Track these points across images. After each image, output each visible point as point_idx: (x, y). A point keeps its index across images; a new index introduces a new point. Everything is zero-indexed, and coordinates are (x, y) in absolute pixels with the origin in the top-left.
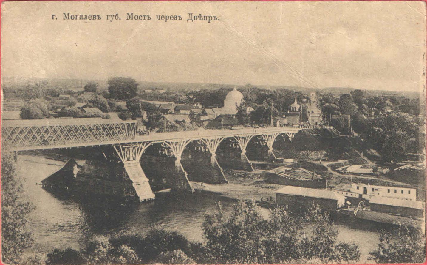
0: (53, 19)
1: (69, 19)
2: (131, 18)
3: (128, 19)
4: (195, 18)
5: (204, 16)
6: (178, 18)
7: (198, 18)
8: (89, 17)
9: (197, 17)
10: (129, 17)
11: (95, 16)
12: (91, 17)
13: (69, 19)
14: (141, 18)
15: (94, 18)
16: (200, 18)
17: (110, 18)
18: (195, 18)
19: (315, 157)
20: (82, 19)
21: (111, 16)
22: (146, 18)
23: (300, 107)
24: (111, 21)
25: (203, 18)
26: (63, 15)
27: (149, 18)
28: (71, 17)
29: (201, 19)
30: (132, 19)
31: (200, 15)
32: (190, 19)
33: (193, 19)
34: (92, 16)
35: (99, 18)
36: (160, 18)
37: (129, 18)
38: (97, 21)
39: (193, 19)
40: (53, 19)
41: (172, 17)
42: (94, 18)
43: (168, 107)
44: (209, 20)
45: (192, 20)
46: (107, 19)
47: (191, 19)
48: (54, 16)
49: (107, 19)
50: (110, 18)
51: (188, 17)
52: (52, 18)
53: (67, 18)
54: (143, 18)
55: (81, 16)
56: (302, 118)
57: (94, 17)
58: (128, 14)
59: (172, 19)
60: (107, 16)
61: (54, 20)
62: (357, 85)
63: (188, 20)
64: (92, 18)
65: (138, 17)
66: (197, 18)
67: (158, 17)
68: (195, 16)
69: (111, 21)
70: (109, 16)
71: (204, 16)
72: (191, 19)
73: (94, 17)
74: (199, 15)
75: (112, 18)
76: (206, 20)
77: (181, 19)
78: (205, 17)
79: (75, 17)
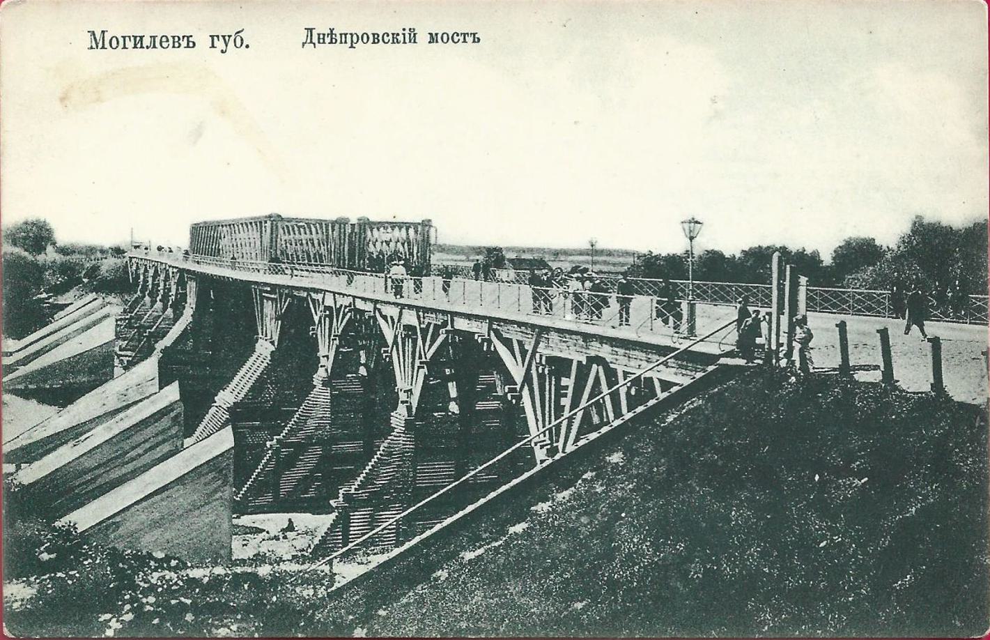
2: (100, 45)
3: (92, 48)
4: (322, 38)
5: (341, 34)
7: (328, 40)
8: (161, 42)
9: (324, 35)
10: (94, 42)
11: (176, 39)
12: (168, 41)
13: (103, 47)
14: (456, 39)
15: (177, 45)
16: (332, 39)
17: (220, 44)
18: (322, 38)
19: (249, 553)
20: (142, 47)
22: (469, 39)
23: (12, 474)
25: (338, 38)
26: (429, 36)
28: (368, 38)
29: (334, 41)
30: (437, 42)
31: (332, 30)
32: (309, 41)
33: (315, 39)
34: (171, 40)
35: (191, 45)
36: (380, 38)
37: (94, 46)
38: (183, 52)
39: (315, 39)
41: (164, 39)
42: (177, 45)
44: (352, 41)
45: (314, 44)
47: (311, 42)
48: (215, 38)
49: (213, 46)
50: (220, 44)
53: (100, 45)
54: (462, 38)
57: (176, 41)
58: (431, 34)
59: (165, 45)
60: (212, 37)
63: (304, 44)
65: (358, 36)
66: (324, 39)
67: (191, 44)
68: (319, 35)
69: (477, 40)
71: (341, 34)
72: (311, 42)
73: (176, 41)
74: (329, 32)
76: (346, 42)
78: (343, 36)
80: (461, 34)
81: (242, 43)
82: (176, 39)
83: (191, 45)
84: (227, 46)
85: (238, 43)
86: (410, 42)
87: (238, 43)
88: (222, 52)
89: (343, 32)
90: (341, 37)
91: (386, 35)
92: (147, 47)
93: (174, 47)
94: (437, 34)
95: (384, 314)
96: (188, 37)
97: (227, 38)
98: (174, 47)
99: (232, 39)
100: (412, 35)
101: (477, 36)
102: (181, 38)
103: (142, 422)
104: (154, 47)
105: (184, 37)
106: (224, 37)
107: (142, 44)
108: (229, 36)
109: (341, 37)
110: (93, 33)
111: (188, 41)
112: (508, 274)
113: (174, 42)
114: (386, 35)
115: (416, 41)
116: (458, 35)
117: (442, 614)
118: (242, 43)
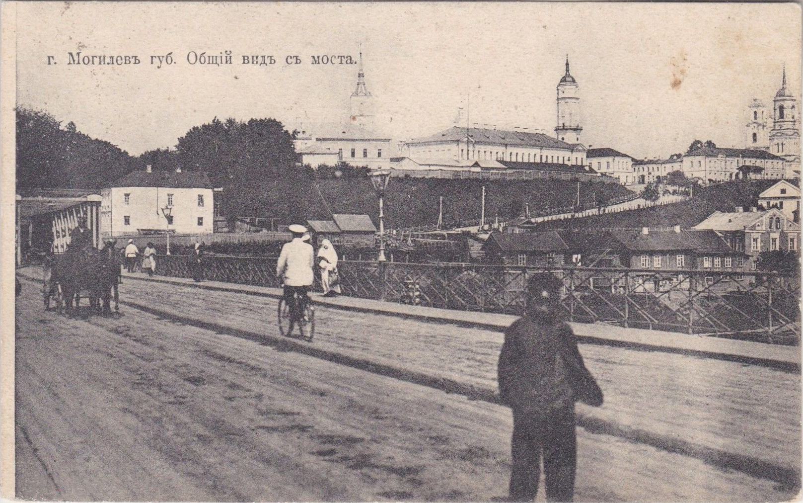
0: (49, 63)
1: (79, 63)
3: (70, 64)
6: (268, 61)
8: (117, 60)
10: (71, 59)
11: (127, 58)
12: (122, 59)
13: (79, 63)
15: (128, 62)
17: (156, 60)
20: (104, 64)
21: (159, 57)
24: (159, 67)
27: (137, 61)
34: (123, 58)
35: (137, 61)
37: (72, 62)
40: (49, 63)
41: (119, 58)
42: (128, 62)
43: (413, 354)
46: (152, 63)
48: (51, 58)
49: (152, 63)
50: (156, 60)
51: (67, 58)
52: (48, 63)
55: (229, 62)
56: (375, 296)
57: (127, 60)
58: (313, 57)
59: (119, 62)
60: (152, 57)
61: (52, 66)
62: (322, 361)
64: (124, 61)
67: (273, 62)
70: (95, 58)
75: (161, 62)
77: (139, 62)
79: (91, 58)
80: (133, 57)
81: (172, 61)
82: (127, 58)
83: (137, 61)
84: (161, 62)
85: (169, 61)
86: (227, 62)
87: (169, 61)
88: (159, 67)
89: (245, 55)
90: (253, 59)
91: (289, 57)
92: (108, 64)
93: (125, 63)
94: (318, 57)
95: (668, 158)
96: (271, 57)
97: (161, 58)
98: (125, 63)
99: (165, 58)
100: (228, 58)
101: (272, 58)
102: (91, 58)
103: (359, 231)
104: (113, 63)
105: (268, 57)
106: (159, 57)
107: (104, 62)
108: (163, 57)
109: (253, 59)
110: (71, 54)
111: (136, 60)
112: (755, 140)
113: (126, 60)
114: (289, 57)
115: (150, 58)
116: (291, 58)
117: (117, 428)
118: (172, 61)
